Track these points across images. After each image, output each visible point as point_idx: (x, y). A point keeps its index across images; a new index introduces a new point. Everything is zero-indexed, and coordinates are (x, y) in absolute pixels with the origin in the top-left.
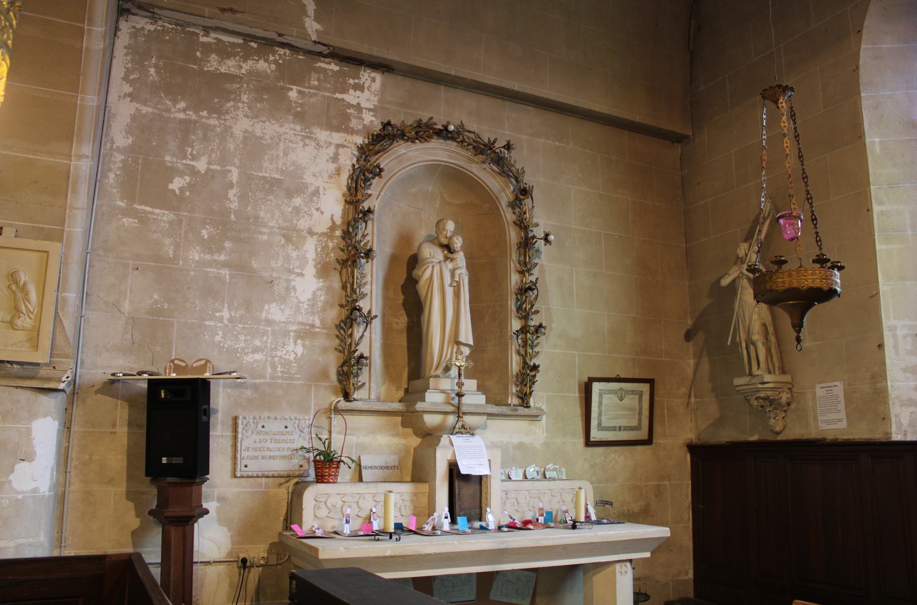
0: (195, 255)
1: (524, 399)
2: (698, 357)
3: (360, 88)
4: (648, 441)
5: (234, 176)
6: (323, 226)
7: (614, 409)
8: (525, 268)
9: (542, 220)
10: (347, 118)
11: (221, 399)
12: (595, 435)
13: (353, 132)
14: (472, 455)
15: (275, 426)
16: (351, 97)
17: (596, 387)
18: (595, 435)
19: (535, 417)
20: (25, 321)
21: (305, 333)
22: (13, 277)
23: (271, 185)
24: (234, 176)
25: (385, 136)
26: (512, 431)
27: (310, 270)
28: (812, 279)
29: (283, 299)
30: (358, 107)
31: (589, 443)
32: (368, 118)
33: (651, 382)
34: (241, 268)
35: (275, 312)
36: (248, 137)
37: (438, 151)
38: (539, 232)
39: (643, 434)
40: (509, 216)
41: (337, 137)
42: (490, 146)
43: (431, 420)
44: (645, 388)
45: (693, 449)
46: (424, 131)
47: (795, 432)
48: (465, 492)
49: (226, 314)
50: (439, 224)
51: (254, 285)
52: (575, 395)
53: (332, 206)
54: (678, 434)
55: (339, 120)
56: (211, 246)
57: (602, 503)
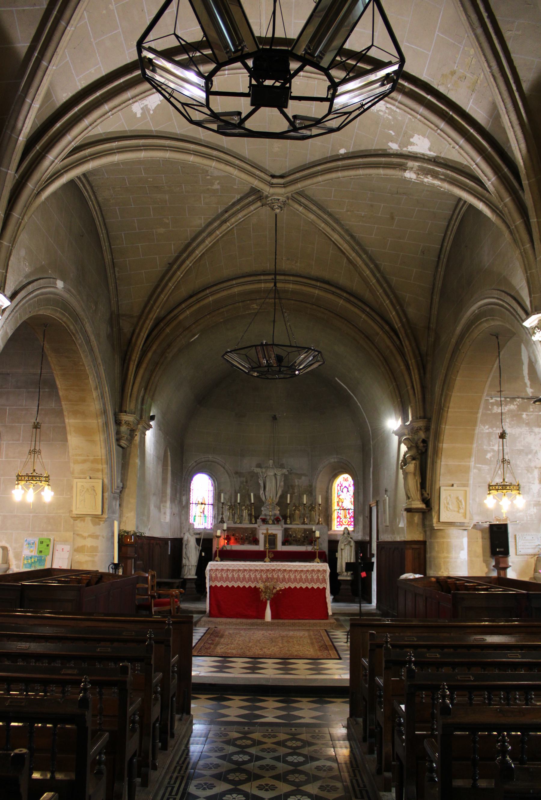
17: (100, 513)
20: (462, 511)
22: (457, 498)
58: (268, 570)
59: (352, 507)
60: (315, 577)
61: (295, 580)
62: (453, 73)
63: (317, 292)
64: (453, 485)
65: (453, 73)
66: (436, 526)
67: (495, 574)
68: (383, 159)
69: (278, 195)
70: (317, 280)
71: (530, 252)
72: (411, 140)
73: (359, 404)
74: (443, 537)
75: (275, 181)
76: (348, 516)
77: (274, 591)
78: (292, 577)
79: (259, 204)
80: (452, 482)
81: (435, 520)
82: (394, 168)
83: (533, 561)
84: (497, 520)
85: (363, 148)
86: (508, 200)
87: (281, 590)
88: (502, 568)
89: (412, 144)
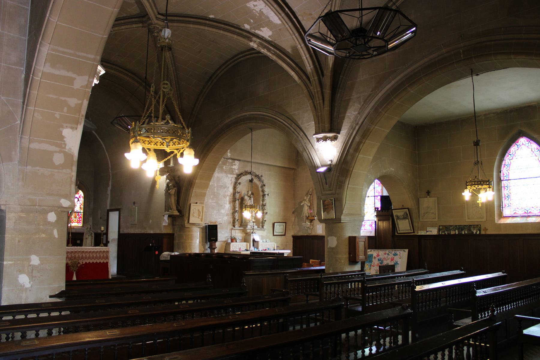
0: (210, 201)
1: (263, 227)
2: (295, 217)
3: (235, 165)
4: (285, 235)
5: (216, 185)
6: (229, 194)
7: (279, 228)
8: (263, 200)
9: (267, 190)
10: (233, 171)
11: (218, 227)
12: (275, 234)
13: (234, 174)
14: (257, 237)
15: (223, 232)
16: (234, 167)
17: (276, 224)
18: (275, 234)
19: (264, 230)
20: (200, 217)
21: (227, 215)
22: (199, 210)
23: (221, 187)
24: (216, 185)
25: (239, 176)
26: (264, 233)
27: (228, 203)
28: (312, 218)
29: (224, 209)
30: (235, 169)
31: (274, 235)
32: (237, 171)
33: (286, 223)
34: (217, 203)
35: (223, 211)
36: (218, 177)
37: (249, 177)
38: (266, 193)
39: (284, 234)
40: (260, 189)
41: (231, 176)
42: (258, 176)
43: (248, 231)
44: (284, 224)
45: (293, 237)
46: (246, 173)
47: (313, 234)
48: (255, 244)
49: (215, 212)
50: (248, 192)
51: (221, 206)
52: (271, 226)
53: (231, 190)
54: (290, 234)
55: (231, 172)
56: (213, 199)
57: (277, 247)
58: (72, 252)
59: (82, 211)
60: (102, 255)
61: (89, 258)
62: (311, 14)
63: (128, 79)
64: (197, 203)
65: (311, 14)
66: (187, 225)
67: (208, 251)
68: (237, 30)
69: (159, 25)
70: (129, 71)
71: (322, 104)
72: (261, 29)
73: (104, 146)
74: (189, 232)
75: (159, 16)
76: (78, 217)
77: (79, 265)
78: (88, 256)
79: (141, 25)
80: (196, 201)
81: (186, 222)
82: (244, 38)
83: (224, 244)
84: (211, 223)
85: (226, 20)
86: (316, 78)
87: (83, 264)
88: (212, 248)
89: (261, 30)
